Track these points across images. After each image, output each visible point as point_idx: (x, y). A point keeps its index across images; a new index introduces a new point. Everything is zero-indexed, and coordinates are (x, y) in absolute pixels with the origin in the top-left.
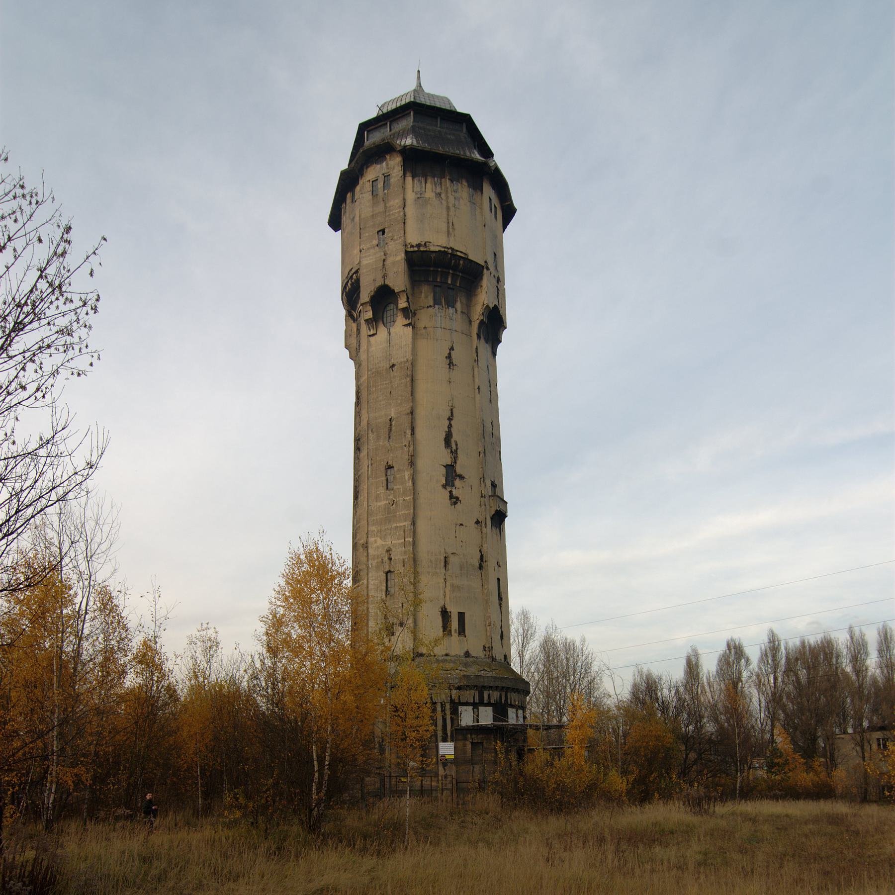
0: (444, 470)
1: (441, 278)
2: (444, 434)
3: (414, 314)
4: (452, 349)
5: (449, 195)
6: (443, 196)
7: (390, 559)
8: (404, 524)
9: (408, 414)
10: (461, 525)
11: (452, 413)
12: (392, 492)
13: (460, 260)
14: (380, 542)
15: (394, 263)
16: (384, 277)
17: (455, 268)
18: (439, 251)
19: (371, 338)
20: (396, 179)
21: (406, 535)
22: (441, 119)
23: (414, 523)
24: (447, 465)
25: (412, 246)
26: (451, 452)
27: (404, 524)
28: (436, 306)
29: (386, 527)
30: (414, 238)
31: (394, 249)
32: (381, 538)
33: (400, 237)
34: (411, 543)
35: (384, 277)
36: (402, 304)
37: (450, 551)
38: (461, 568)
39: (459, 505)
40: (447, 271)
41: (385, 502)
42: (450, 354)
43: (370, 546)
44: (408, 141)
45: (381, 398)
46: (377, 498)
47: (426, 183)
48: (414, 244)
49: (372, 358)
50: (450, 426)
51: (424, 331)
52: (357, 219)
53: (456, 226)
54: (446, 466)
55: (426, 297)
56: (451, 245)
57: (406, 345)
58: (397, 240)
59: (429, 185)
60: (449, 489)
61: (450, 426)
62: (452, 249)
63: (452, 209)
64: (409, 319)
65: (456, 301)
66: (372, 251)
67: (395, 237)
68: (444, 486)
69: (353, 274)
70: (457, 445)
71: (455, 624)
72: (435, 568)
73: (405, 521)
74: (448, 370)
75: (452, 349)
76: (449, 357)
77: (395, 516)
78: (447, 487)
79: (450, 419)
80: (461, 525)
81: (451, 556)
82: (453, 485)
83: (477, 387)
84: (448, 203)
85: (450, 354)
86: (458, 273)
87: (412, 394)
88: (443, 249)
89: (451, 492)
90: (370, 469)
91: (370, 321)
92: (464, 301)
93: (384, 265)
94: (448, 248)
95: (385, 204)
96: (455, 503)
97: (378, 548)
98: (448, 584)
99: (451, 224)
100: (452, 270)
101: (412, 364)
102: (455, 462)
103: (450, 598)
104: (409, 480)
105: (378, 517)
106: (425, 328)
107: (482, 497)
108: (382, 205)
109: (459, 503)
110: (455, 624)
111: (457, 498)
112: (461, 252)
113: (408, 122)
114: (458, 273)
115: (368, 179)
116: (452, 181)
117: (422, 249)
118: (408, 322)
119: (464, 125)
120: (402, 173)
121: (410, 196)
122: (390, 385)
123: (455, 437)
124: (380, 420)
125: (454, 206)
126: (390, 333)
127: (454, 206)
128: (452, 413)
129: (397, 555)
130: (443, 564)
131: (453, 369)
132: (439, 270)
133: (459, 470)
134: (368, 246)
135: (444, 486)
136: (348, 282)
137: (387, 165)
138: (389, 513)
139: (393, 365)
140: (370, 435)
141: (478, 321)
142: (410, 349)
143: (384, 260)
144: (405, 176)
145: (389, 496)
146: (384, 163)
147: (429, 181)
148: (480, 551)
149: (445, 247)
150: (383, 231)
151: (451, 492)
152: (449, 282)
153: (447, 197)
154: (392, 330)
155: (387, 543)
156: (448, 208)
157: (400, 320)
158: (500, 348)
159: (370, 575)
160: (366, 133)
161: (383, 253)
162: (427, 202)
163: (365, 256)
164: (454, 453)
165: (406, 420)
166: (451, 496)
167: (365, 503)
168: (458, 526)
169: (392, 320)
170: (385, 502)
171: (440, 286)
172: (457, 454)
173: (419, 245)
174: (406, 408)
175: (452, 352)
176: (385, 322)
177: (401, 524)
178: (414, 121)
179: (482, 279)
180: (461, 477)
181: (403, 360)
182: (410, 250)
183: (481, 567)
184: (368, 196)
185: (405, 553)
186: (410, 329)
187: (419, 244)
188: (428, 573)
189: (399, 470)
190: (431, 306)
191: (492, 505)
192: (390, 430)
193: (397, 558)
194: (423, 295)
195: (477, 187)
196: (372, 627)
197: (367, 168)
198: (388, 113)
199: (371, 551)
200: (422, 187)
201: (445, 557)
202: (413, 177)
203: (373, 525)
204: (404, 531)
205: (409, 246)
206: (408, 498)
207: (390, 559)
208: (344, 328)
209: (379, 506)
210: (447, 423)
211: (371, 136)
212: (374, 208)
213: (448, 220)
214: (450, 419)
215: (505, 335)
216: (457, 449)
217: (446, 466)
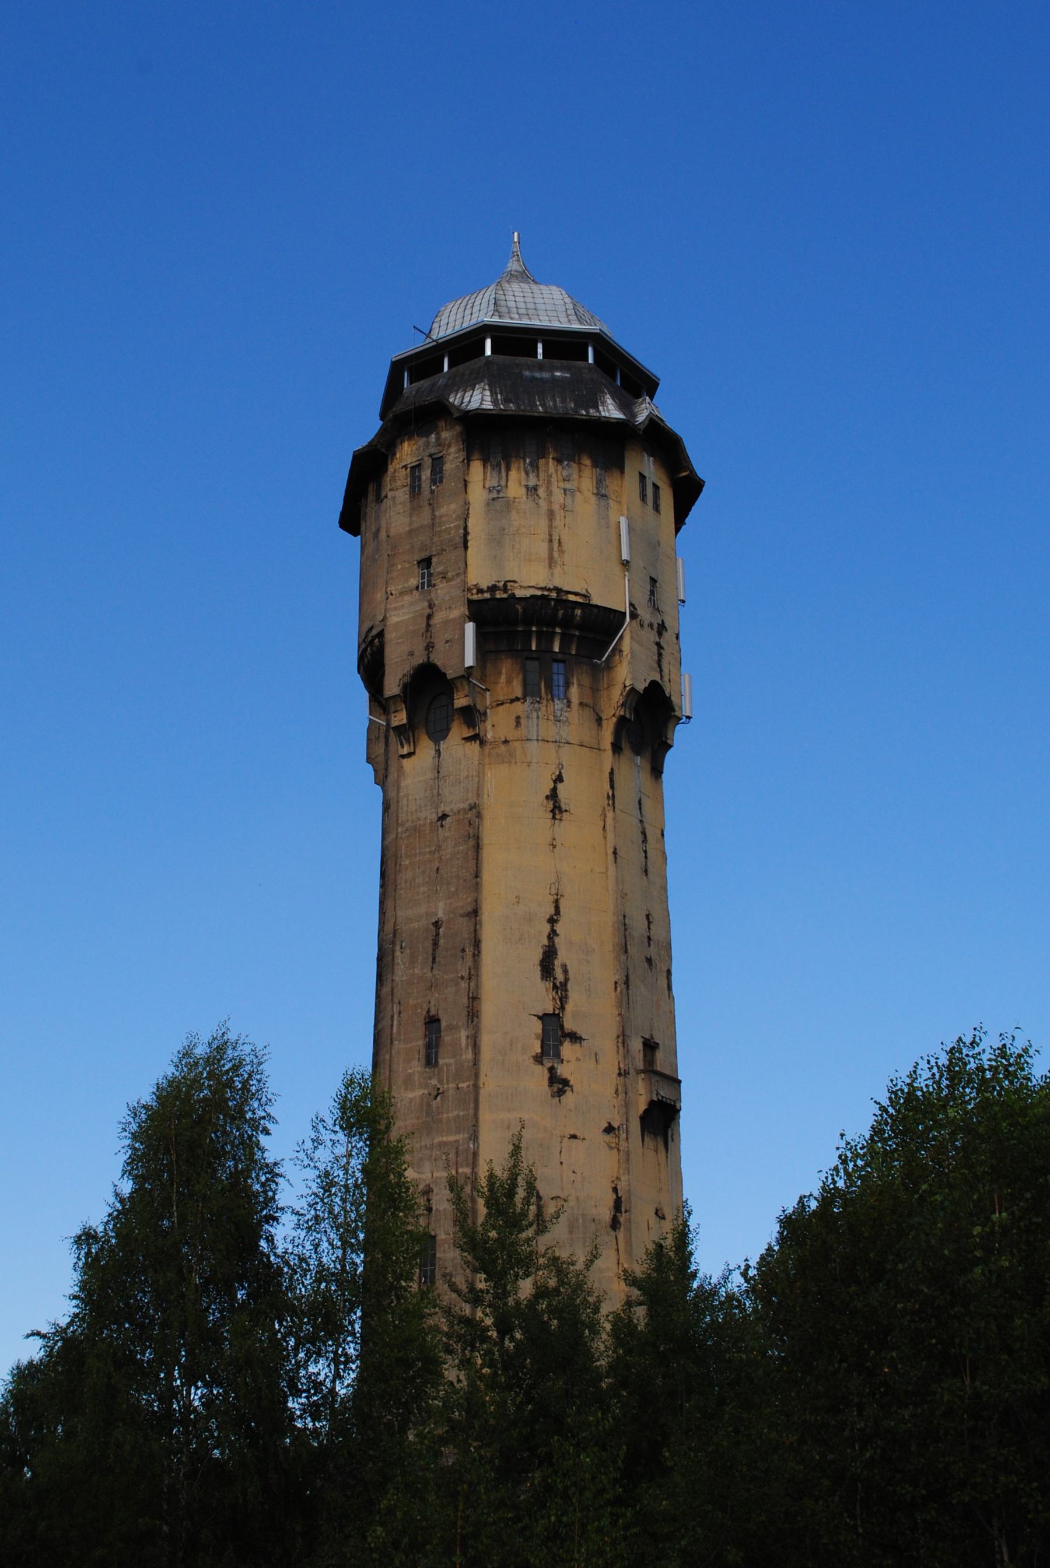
0: (537, 1027)
4: (559, 779)
6: (541, 492)
10: (574, 1137)
13: (573, 609)
16: (429, 647)
17: (567, 623)
18: (533, 597)
24: (545, 1014)
25: (480, 591)
26: (555, 987)
31: (447, 598)
35: (429, 647)
39: (569, 1098)
40: (550, 630)
42: (554, 790)
46: (408, 1082)
47: (508, 469)
48: (484, 586)
53: (566, 546)
54: (543, 1018)
55: (509, 681)
56: (558, 582)
57: (467, 777)
62: (558, 590)
63: (559, 514)
65: (567, 684)
66: (407, 598)
67: (450, 575)
68: (538, 1059)
70: (566, 972)
73: (459, 1133)
74: (549, 822)
75: (559, 779)
76: (553, 795)
79: (552, 921)
80: (574, 1137)
82: (557, 1055)
83: (610, 851)
85: (554, 790)
87: (477, 875)
88: (539, 593)
89: (552, 1070)
93: (428, 625)
94: (549, 590)
96: (560, 1093)
99: (556, 545)
102: (563, 1008)
104: (467, 1048)
105: (408, 1122)
109: (569, 1093)
111: (565, 1082)
112: (576, 594)
116: (559, 461)
117: (499, 595)
118: (472, 734)
120: (462, 455)
123: (563, 956)
124: (416, 925)
125: (564, 507)
131: (561, 820)
135: (538, 1059)
139: (444, 816)
141: (614, 720)
143: (429, 617)
145: (430, 1078)
148: (615, 1190)
151: (552, 1070)
153: (550, 493)
163: (395, 609)
164: (561, 990)
168: (566, 1140)
172: (566, 990)
173: (493, 589)
180: (575, 1038)
181: (462, 806)
183: (615, 1224)
190: (517, 699)
193: (441, 1208)
194: (503, 678)
200: (500, 478)
202: (485, 461)
205: (475, 591)
209: (411, 1099)
210: (547, 928)
212: (414, 518)
213: (550, 535)
214: (552, 921)
216: (567, 980)
217: (543, 1018)
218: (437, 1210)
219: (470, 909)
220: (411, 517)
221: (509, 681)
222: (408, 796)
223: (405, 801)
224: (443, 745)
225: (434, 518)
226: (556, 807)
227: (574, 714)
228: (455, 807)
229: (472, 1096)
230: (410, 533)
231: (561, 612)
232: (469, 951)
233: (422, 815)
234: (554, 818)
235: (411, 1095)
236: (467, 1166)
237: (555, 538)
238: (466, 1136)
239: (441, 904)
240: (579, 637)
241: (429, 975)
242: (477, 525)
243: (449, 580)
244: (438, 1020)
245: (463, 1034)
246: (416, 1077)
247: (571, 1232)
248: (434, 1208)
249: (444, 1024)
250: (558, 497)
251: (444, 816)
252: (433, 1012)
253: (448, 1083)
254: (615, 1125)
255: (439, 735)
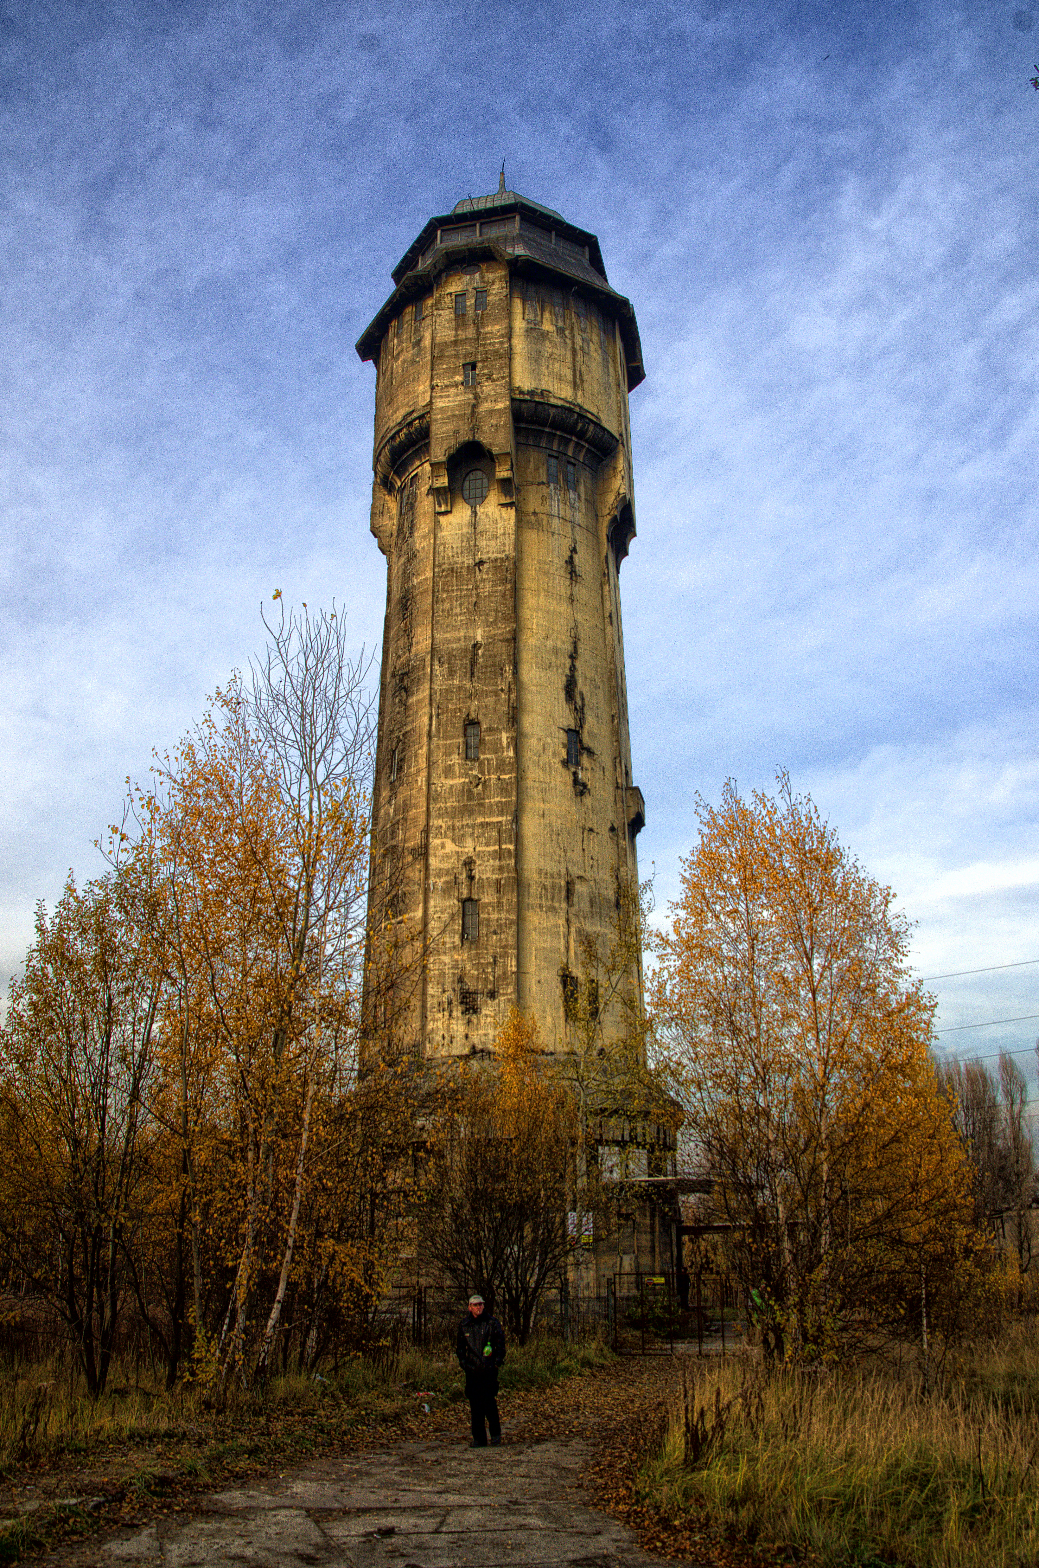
1: (559, 446)
2: (564, 679)
3: (518, 490)
4: (574, 550)
5: (576, 334)
6: (567, 332)
7: (471, 878)
8: (500, 819)
9: (507, 640)
10: (591, 830)
11: (575, 648)
12: (477, 764)
14: (450, 847)
15: (491, 412)
16: (474, 429)
17: (581, 435)
18: (562, 407)
19: (441, 518)
20: (497, 298)
21: (503, 839)
22: (557, 235)
23: (517, 819)
24: (570, 730)
26: (576, 709)
27: (500, 819)
28: (552, 485)
29: (465, 823)
30: (524, 380)
31: (493, 393)
32: (454, 840)
33: (503, 378)
34: (513, 853)
35: (474, 429)
36: (503, 472)
37: (575, 871)
38: (592, 902)
39: (588, 800)
41: (462, 780)
42: (571, 558)
43: (431, 852)
44: (520, 251)
45: (458, 611)
46: (448, 771)
47: (543, 311)
49: (442, 548)
50: (573, 668)
51: (533, 518)
52: (427, 342)
53: (585, 378)
54: (568, 731)
55: (536, 469)
57: (504, 534)
58: (498, 380)
59: (547, 315)
60: (573, 770)
61: (573, 668)
62: (581, 408)
63: (579, 353)
64: (511, 497)
66: (452, 390)
67: (495, 377)
69: (415, 420)
70: (583, 699)
71: (582, 1003)
72: (552, 900)
73: (502, 815)
75: (574, 550)
76: (570, 561)
77: (483, 805)
78: (570, 765)
81: (577, 881)
82: (578, 764)
83: (607, 615)
84: (573, 343)
85: (571, 558)
86: (583, 443)
89: (575, 774)
90: (434, 722)
91: (442, 492)
92: (589, 482)
95: (478, 329)
96: (581, 794)
97: (448, 856)
98: (573, 930)
100: (577, 437)
101: (515, 563)
102: (581, 727)
103: (575, 953)
104: (508, 747)
105: (449, 804)
106: (535, 513)
107: (617, 787)
108: (471, 332)
109: (587, 794)
110: (582, 1003)
111: (585, 786)
112: (592, 414)
113: (515, 226)
114: (583, 443)
115: (449, 291)
116: (578, 316)
118: (508, 501)
119: (587, 249)
120: (505, 292)
121: (519, 324)
122: (474, 592)
124: (455, 646)
125: (582, 349)
126: (475, 513)
127: (582, 349)
128: (575, 648)
129: (485, 870)
130: (563, 894)
132: (558, 433)
133: (586, 740)
134: (446, 382)
136: (401, 430)
137: (482, 277)
138: (470, 799)
140: (437, 667)
141: (609, 517)
142: (512, 541)
143: (474, 406)
144: (510, 297)
145: (471, 769)
146: (477, 276)
147: (548, 309)
149: (570, 403)
150: (474, 367)
151: (575, 774)
152: (570, 454)
153: (573, 337)
154: (480, 510)
155: (466, 850)
156: (574, 352)
157: (494, 498)
158: (625, 562)
159: (432, 903)
160: (439, 232)
161: (471, 396)
162: (544, 335)
163: (441, 397)
164: (579, 712)
165: (502, 650)
166: (576, 781)
167: (422, 780)
169: (479, 494)
170: (462, 780)
171: (557, 458)
173: (532, 393)
174: (504, 629)
175: (576, 557)
176: (466, 497)
177: (494, 819)
178: (521, 229)
179: (615, 458)
180: (590, 752)
181: (499, 556)
182: (518, 397)
183: (618, 905)
184: (447, 315)
185: (501, 869)
186: (511, 513)
187: (533, 391)
188: (541, 906)
189: (490, 730)
190: (543, 483)
191: (631, 804)
192: (473, 663)
193: (484, 877)
195: (607, 331)
196: (433, 996)
197: (447, 276)
198: (480, 212)
199: (433, 862)
200: (536, 316)
201: (568, 883)
202: (524, 301)
203: (439, 816)
204: (499, 832)
206: (507, 777)
207: (471, 878)
208: (370, 501)
209: (452, 786)
211: (445, 238)
212: (459, 332)
214: (573, 657)
215: (633, 545)
216: (583, 705)
217: (568, 731)
218: (480, 878)
219: (509, 636)
220: (456, 330)
221: (536, 469)
222: (444, 544)
223: (442, 548)
224: (480, 510)
225: (478, 333)
226: (573, 573)
227: (582, 506)
228: (493, 556)
229: (514, 786)
230: (455, 343)
231: (580, 425)
232: (508, 668)
233: (459, 560)
234: (571, 579)
235: (451, 782)
236: (511, 843)
237: (578, 368)
238: (509, 818)
239: (479, 632)
240: (588, 450)
241: (468, 686)
242: (519, 344)
243: (493, 381)
244: (478, 723)
245: (504, 737)
246: (457, 768)
247: (592, 907)
248: (477, 877)
249: (484, 726)
250: (579, 341)
251: (481, 563)
252: (473, 715)
253: (489, 774)
254: (616, 826)
255: (475, 500)
